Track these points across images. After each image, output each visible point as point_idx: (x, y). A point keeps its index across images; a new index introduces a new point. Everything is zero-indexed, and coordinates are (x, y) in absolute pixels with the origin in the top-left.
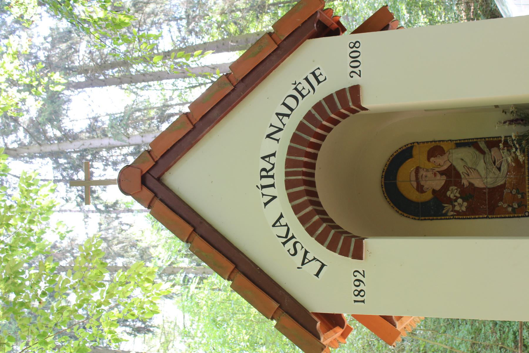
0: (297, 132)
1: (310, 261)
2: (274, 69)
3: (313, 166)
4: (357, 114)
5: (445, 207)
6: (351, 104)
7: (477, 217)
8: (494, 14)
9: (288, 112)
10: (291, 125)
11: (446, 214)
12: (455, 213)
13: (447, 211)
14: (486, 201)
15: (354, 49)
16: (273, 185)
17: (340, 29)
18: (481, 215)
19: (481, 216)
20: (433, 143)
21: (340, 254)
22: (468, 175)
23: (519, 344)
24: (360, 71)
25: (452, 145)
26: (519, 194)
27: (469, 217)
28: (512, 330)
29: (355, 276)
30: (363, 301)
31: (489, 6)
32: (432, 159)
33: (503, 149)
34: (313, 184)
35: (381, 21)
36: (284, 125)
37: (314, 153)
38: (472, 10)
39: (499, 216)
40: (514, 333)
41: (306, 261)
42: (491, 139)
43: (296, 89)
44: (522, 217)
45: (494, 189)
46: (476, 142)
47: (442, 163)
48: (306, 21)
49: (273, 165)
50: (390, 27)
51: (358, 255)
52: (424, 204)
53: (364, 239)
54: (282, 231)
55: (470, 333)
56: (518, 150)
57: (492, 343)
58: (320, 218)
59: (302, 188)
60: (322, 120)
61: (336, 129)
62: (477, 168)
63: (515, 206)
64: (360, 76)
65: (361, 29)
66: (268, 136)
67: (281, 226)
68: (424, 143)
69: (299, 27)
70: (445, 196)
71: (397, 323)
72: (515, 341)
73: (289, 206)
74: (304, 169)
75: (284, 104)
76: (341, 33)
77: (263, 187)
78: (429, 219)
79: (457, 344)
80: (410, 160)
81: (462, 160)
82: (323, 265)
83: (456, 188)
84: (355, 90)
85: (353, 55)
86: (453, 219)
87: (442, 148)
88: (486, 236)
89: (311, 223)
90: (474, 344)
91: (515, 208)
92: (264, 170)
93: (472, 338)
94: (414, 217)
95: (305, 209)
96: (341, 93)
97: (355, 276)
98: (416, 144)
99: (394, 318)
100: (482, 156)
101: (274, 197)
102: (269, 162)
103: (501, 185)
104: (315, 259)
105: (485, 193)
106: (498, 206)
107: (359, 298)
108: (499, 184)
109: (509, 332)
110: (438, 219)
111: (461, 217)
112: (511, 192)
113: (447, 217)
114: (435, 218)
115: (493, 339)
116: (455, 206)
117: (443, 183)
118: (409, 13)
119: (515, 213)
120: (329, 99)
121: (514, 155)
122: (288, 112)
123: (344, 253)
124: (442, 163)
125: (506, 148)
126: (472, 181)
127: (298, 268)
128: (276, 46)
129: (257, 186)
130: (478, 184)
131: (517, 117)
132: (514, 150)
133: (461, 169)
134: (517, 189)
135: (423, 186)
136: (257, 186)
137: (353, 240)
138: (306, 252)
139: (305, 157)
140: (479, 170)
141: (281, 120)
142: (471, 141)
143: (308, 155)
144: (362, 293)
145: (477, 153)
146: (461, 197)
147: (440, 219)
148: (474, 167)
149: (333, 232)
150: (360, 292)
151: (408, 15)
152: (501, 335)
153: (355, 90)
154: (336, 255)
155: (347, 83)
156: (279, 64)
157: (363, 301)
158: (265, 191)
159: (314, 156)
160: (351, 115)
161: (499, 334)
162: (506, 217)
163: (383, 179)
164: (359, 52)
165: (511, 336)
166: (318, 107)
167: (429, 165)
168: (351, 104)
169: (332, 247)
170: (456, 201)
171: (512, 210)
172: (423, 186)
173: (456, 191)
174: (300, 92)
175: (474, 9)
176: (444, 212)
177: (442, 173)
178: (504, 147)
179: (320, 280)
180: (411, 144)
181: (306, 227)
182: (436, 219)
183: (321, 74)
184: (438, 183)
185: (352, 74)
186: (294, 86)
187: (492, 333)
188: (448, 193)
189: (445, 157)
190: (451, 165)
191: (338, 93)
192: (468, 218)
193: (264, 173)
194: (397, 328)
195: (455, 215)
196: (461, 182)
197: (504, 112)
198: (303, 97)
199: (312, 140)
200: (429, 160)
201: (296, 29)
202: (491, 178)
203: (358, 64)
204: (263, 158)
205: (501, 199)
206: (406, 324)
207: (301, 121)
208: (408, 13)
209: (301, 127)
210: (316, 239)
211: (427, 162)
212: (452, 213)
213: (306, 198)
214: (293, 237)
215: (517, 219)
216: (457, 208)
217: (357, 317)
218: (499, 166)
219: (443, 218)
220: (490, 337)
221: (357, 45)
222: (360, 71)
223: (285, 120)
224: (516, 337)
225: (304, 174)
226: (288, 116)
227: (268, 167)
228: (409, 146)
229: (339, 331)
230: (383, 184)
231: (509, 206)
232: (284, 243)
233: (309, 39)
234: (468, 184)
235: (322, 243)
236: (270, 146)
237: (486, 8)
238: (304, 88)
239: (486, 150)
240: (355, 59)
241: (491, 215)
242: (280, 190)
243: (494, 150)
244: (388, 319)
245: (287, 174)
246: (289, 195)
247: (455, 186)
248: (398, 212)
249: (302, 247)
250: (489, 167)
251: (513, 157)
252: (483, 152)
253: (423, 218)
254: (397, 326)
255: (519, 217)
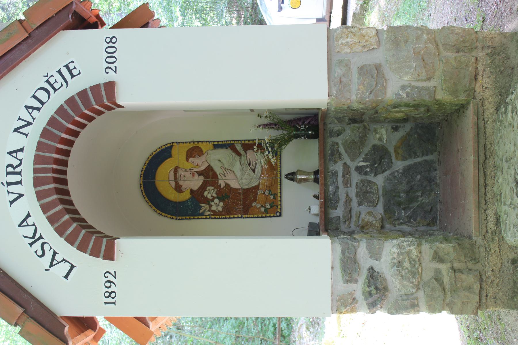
0: (48, 127)
1: (59, 263)
2: (24, 59)
3: (65, 163)
4: (113, 111)
5: (202, 207)
6: (105, 100)
7: (232, 216)
8: (262, 22)
9: (39, 105)
10: (42, 119)
11: (202, 214)
12: (212, 213)
13: (204, 211)
14: (241, 201)
15: (111, 44)
16: (20, 183)
17: (99, 22)
18: (236, 214)
19: (236, 216)
20: (192, 143)
21: (90, 255)
22: (225, 176)
23: (277, 336)
24: (116, 67)
25: (211, 146)
26: (271, 195)
27: (224, 217)
28: (272, 322)
29: (107, 277)
30: (114, 303)
31: (257, 17)
32: (191, 159)
33: (257, 152)
34: (64, 182)
35: (140, 19)
36: (34, 119)
37: (67, 150)
38: (242, 19)
39: (252, 216)
40: (274, 325)
41: (55, 262)
42: (247, 142)
43: (48, 81)
44: (273, 217)
45: (248, 189)
46: (233, 144)
47: (200, 164)
48: (60, 11)
49: (21, 161)
50: (150, 25)
51: (109, 256)
52: (182, 203)
53: (116, 239)
54: (30, 232)
55: (234, 328)
56: (271, 153)
57: (254, 335)
58: (71, 218)
59: (52, 186)
60: (74, 116)
61: (90, 125)
62: (233, 170)
63: (267, 207)
64: (116, 72)
65: (118, 26)
66: (16, 130)
67: (28, 225)
68: (183, 143)
69: (53, 17)
70: (203, 196)
71: (151, 324)
72: (274, 334)
73: (37, 204)
74: (55, 166)
75: (34, 96)
76: (100, 27)
77: (9, 184)
78: (187, 219)
79: (222, 339)
80: (169, 160)
81: (220, 161)
82: (73, 267)
83: (213, 188)
84: (110, 86)
85: (109, 50)
86: (209, 218)
87: (200, 148)
88: (229, 235)
89: (60, 223)
90: (238, 337)
91: (267, 209)
92: (10, 165)
93: (236, 332)
94: (172, 217)
95: (54, 208)
96: (95, 89)
97: (107, 277)
98: (175, 144)
99: (147, 318)
100: (238, 158)
101: (21, 195)
102: (16, 158)
103: (255, 186)
104: (64, 260)
105: (240, 194)
106: (252, 207)
107: (110, 300)
108: (253, 185)
109: (269, 324)
110: (195, 219)
111: (217, 217)
112: (264, 193)
113: (204, 217)
114: (192, 217)
115: (254, 331)
116: (211, 206)
117: (201, 184)
118: (183, 15)
119: (268, 214)
120: (82, 94)
121: (266, 158)
122: (39, 105)
123: (95, 253)
124: (200, 163)
125: (259, 151)
126: (228, 182)
127: (46, 270)
128: (27, 35)
129: (2, 183)
130: (234, 185)
131: (271, 122)
132: (267, 153)
133: (218, 170)
134: (270, 191)
135: (181, 186)
136: (2, 183)
137: (105, 240)
138: (55, 253)
139: (56, 153)
140: (235, 171)
141: (30, 114)
142: (228, 142)
143: (59, 151)
144: (113, 295)
145: (234, 154)
146: (217, 198)
147: (197, 219)
148: (230, 168)
149: (84, 231)
150: (111, 293)
151: (182, 18)
152: (262, 327)
153: (110, 86)
154: (87, 255)
155: (102, 78)
156: (30, 54)
157: (114, 303)
158: (11, 188)
159: (67, 153)
160: (106, 111)
161: (260, 326)
162: (259, 217)
163: (142, 178)
164: (115, 47)
165: (272, 329)
166: (71, 101)
167: (188, 165)
168: (105, 100)
169: (82, 248)
170: (212, 201)
171: (265, 210)
172: (181, 186)
173: (213, 191)
174: (51, 85)
175: (244, 17)
176: (201, 211)
177: (200, 173)
178: (258, 150)
179: (69, 283)
180: (170, 143)
181: (55, 227)
182: (193, 219)
183: (75, 68)
184: (196, 183)
185: (108, 70)
186: (46, 78)
187: (254, 325)
188: (206, 193)
189: (203, 158)
190: (209, 165)
191: (92, 88)
192: (224, 218)
193: (10, 169)
194: (151, 329)
195: (212, 215)
196: (218, 183)
197: (260, 116)
198: (55, 90)
199: (64, 136)
200: (187, 160)
201: (49, 19)
202: (246, 179)
203: (114, 60)
204: (10, 153)
205: (255, 200)
206: (161, 323)
207: (52, 116)
208: (181, 15)
209: (52, 122)
210: (65, 240)
211: (185, 162)
212: (209, 213)
213: (55, 196)
214: (41, 237)
215: (269, 218)
216: (214, 208)
217: (111, 320)
218: (253, 168)
219: (200, 217)
220: (253, 330)
221: (114, 40)
222: (116, 67)
223: (35, 113)
224: (275, 329)
225: (55, 171)
226: (39, 109)
227: (15, 163)
228: (169, 145)
229: (91, 334)
230: (142, 183)
231: (262, 206)
232: (31, 244)
233: (63, 30)
234: (224, 185)
235: (72, 244)
236: (17, 141)
237: (255, 17)
238: (56, 81)
239: (242, 152)
240: (111, 55)
241: (245, 214)
242: (28, 188)
243: (249, 152)
244: (142, 320)
245: (35, 171)
246: (37, 193)
247: (212, 186)
248: (156, 211)
249: (51, 248)
250: (245, 169)
251: (266, 160)
252: (239, 154)
253: (180, 218)
254: (151, 326)
255: (271, 217)
